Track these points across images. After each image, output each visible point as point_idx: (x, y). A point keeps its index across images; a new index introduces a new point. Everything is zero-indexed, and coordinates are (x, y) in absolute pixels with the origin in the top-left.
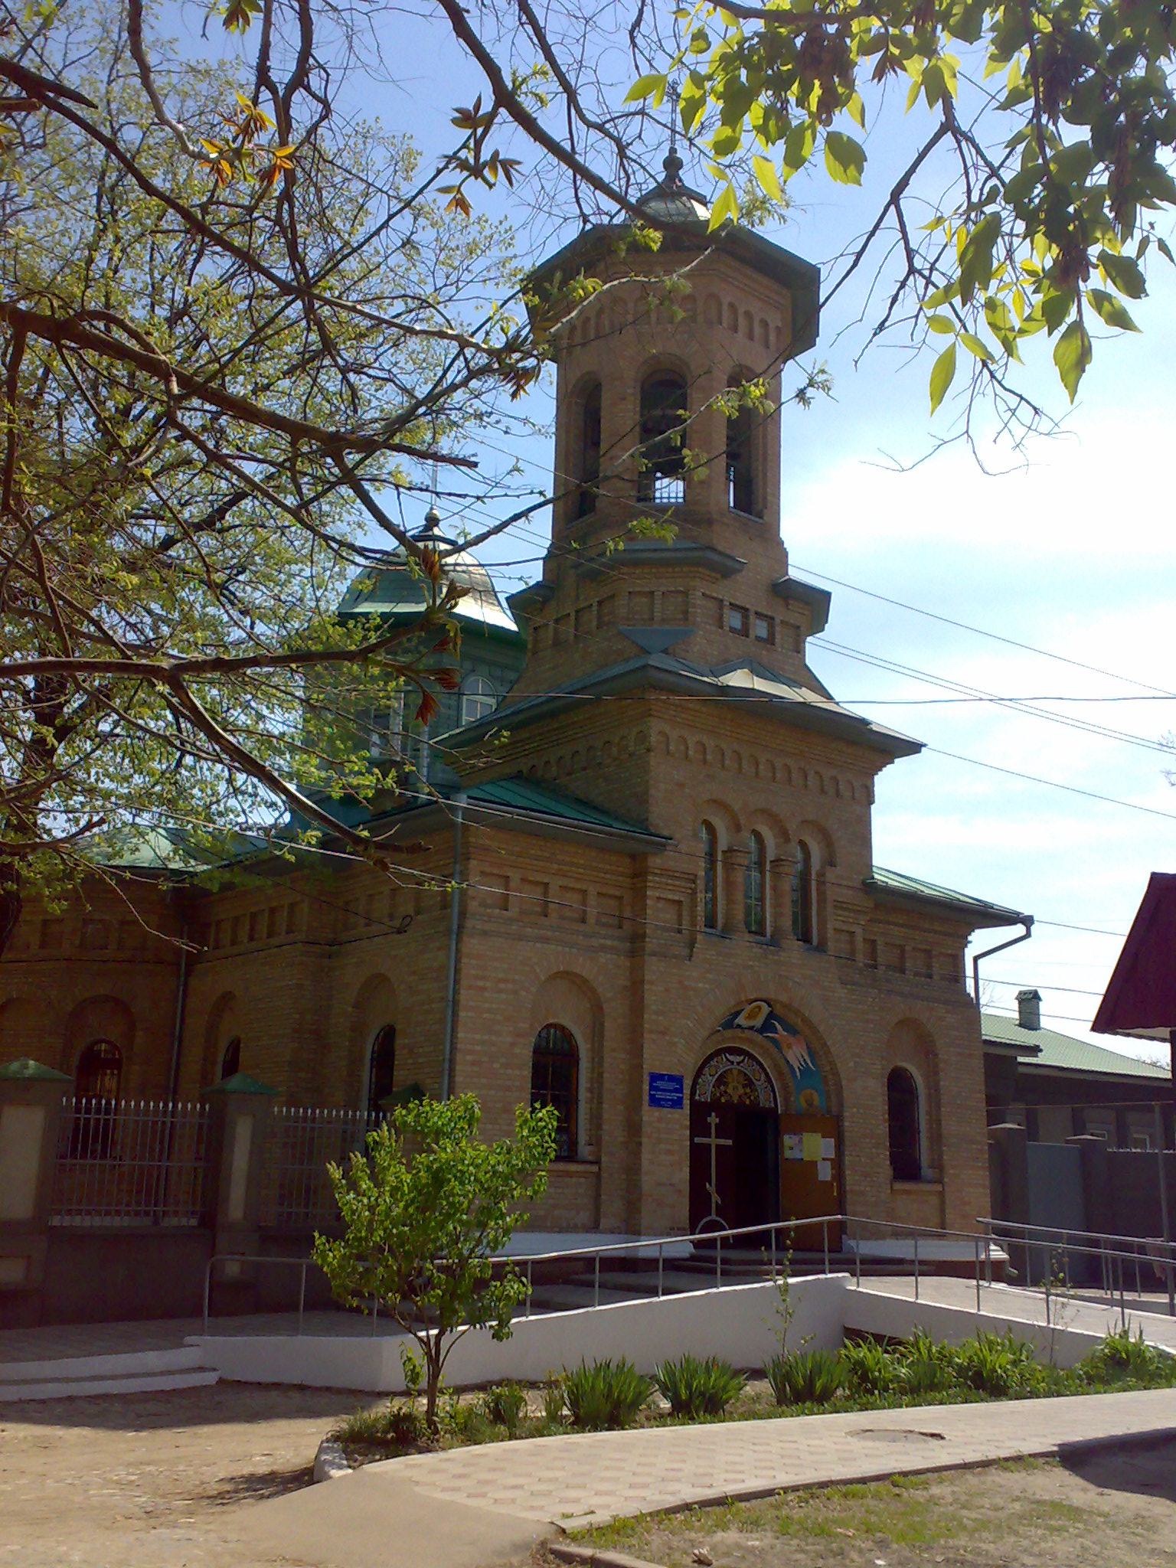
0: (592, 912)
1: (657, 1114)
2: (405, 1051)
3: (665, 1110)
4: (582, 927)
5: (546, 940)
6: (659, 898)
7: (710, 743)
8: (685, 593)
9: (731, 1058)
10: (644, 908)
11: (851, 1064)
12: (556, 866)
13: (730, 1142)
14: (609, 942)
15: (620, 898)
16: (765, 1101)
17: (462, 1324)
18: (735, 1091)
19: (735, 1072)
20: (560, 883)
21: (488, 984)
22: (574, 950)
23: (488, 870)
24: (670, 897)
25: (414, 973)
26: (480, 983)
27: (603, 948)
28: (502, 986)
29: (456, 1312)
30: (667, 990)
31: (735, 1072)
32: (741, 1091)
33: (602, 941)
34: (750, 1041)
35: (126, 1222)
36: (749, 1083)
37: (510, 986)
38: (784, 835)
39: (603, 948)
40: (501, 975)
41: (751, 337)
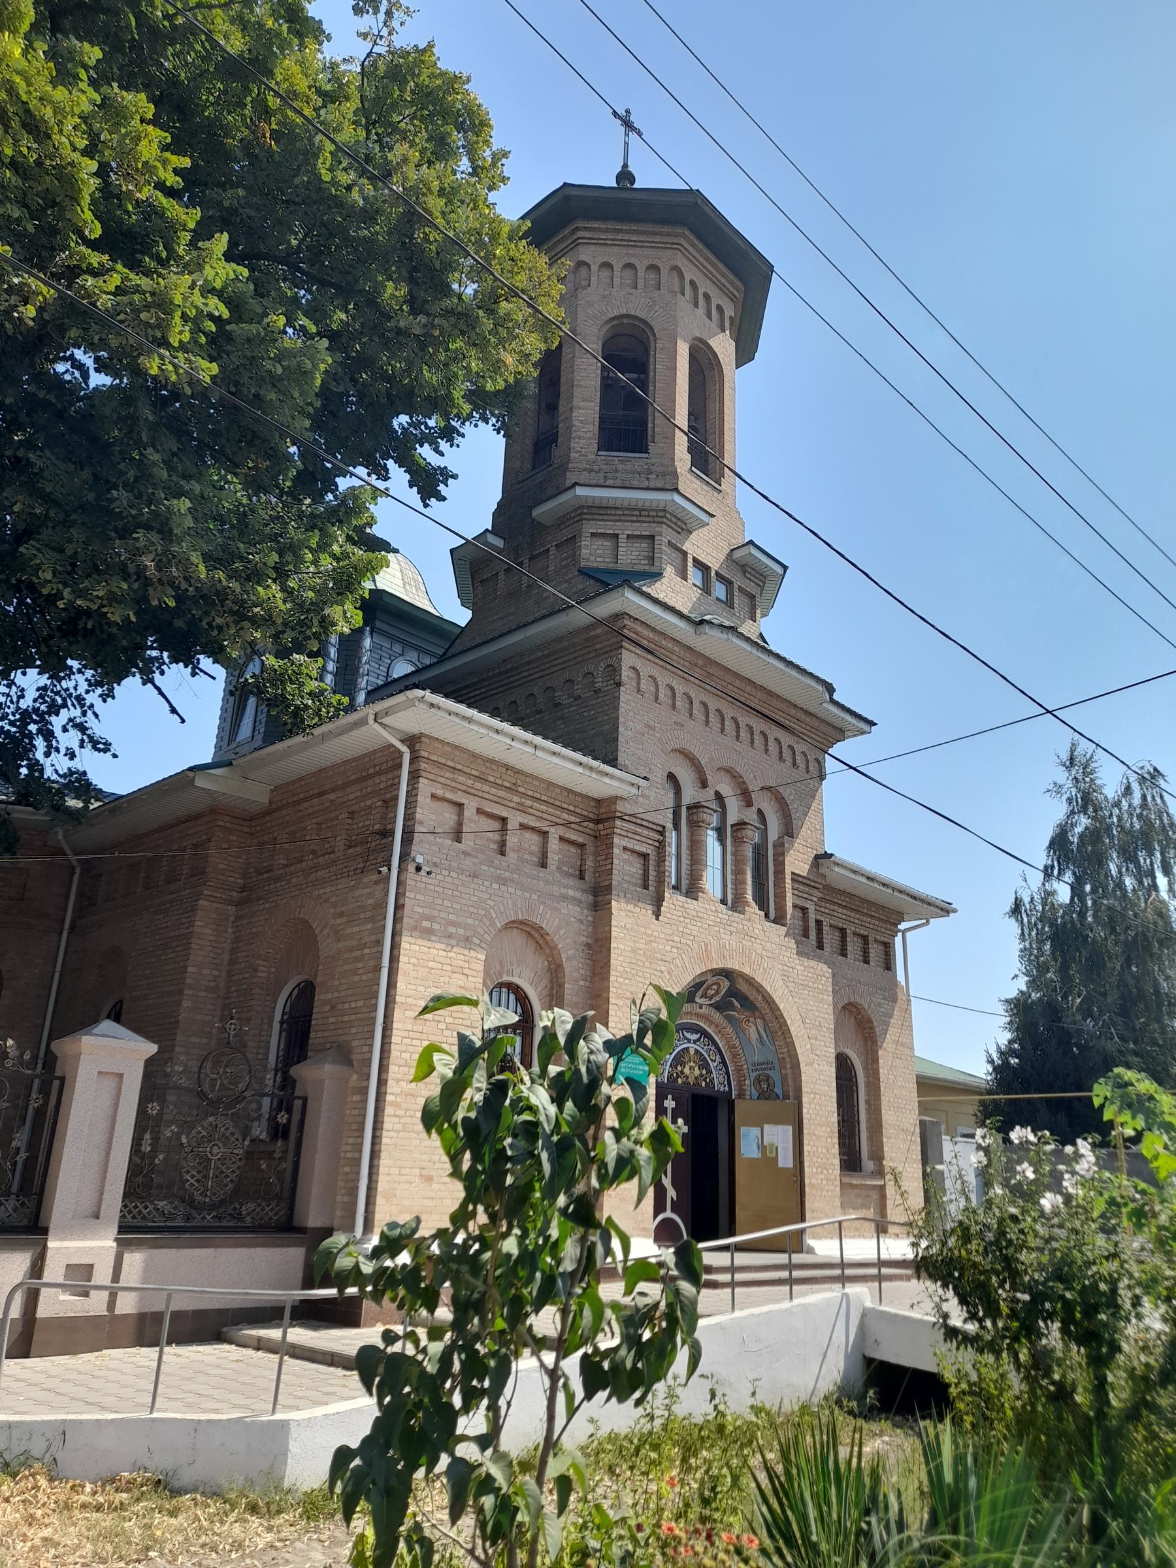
0: (553, 858)
2: (327, 1008)
4: (542, 873)
5: (503, 881)
6: (625, 848)
7: (680, 688)
8: (652, 537)
9: (688, 1035)
10: (609, 857)
11: (808, 1046)
12: (516, 799)
14: (571, 893)
15: (581, 846)
16: (719, 1085)
17: (444, 1382)
18: (691, 1071)
19: (692, 1052)
20: (520, 819)
21: (436, 926)
22: (535, 897)
23: (440, 792)
24: (637, 848)
25: (341, 914)
26: (426, 924)
27: (564, 898)
28: (452, 930)
29: (1044, 1347)
30: (633, 951)
31: (692, 1052)
32: (697, 1072)
33: (563, 891)
34: (708, 1019)
35: (798, 1535)
36: (704, 1065)
37: (461, 931)
38: (746, 797)
39: (564, 898)
40: (452, 917)
41: (709, 316)
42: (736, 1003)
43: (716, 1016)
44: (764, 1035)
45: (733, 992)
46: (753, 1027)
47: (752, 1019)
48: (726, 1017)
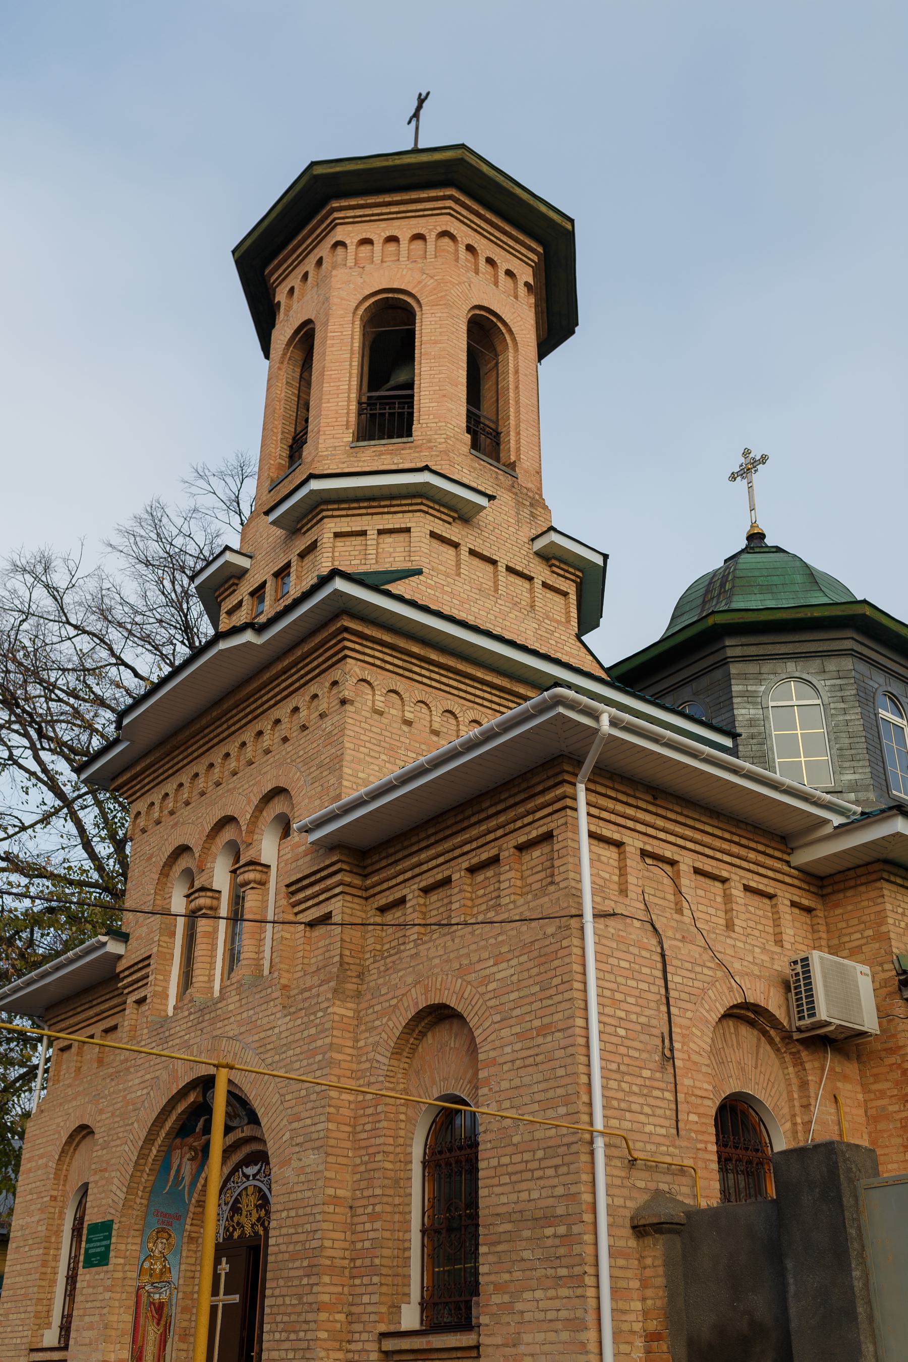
13: (237, 1297)
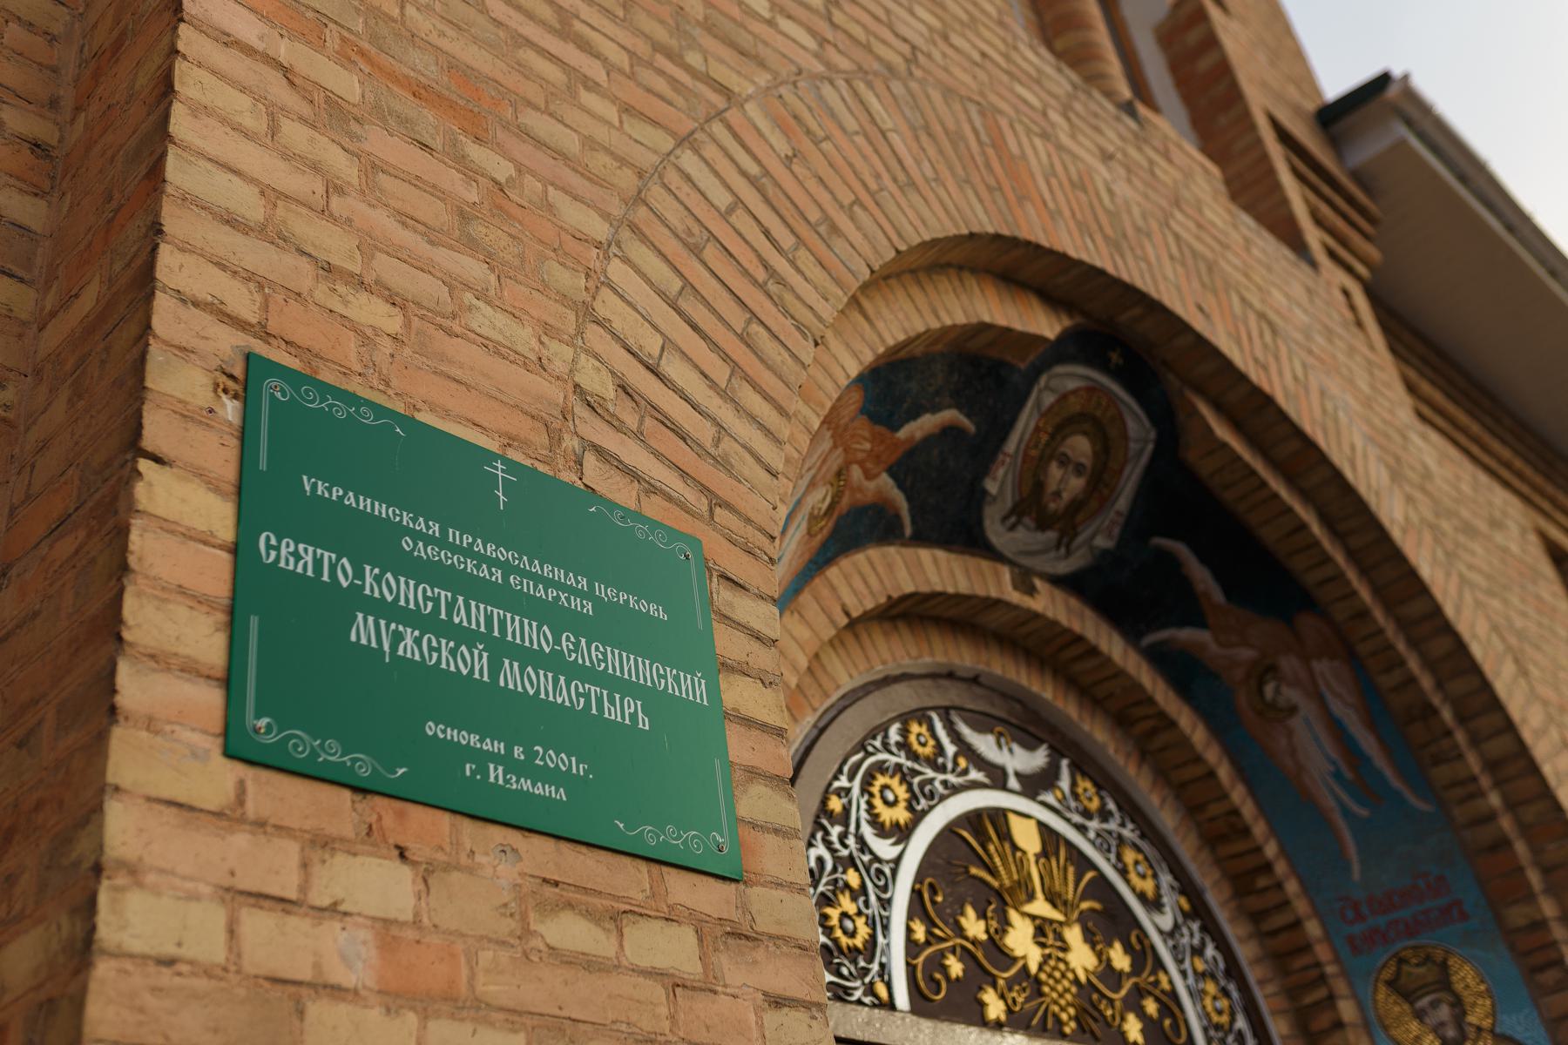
1: (376, 885)
3: (500, 863)
42: (1201, 576)
43: (1113, 646)
44: (1368, 743)
45: (1182, 499)
46: (1307, 708)
47: (1289, 664)
48: (1160, 658)
